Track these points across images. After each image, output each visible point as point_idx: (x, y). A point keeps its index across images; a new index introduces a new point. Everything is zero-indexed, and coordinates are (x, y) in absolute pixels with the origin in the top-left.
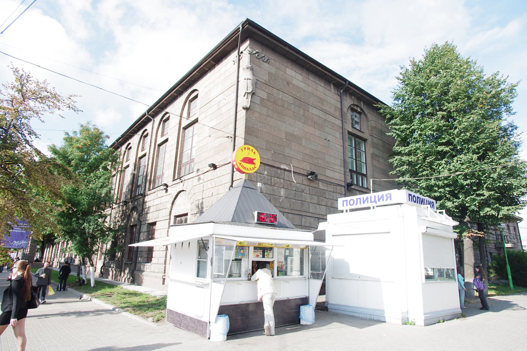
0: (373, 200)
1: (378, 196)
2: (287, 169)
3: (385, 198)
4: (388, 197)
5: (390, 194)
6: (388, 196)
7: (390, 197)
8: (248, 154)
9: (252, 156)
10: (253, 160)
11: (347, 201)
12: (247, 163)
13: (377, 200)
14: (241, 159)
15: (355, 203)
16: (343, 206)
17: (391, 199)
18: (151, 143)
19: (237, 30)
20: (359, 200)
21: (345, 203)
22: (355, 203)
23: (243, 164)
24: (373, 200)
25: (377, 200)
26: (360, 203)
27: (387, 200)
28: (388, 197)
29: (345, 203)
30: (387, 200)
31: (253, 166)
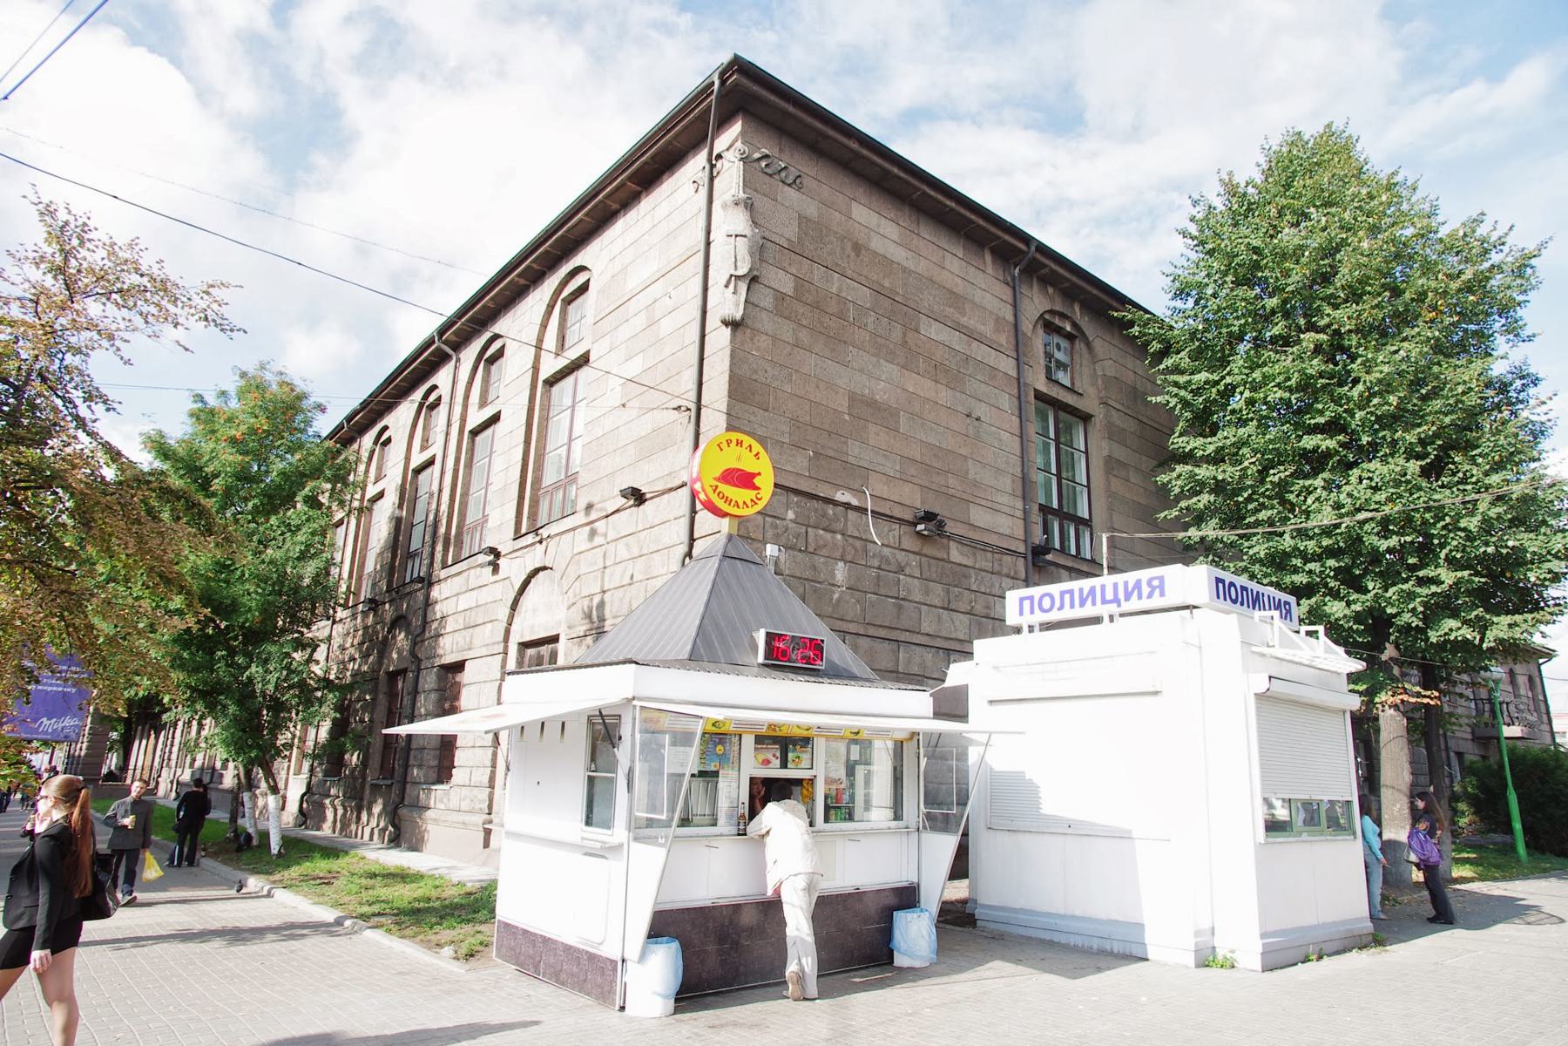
0: (1109, 596)
2: (855, 502)
3: (1146, 590)
4: (1153, 589)
5: (1161, 579)
6: (1156, 583)
8: (739, 459)
9: (749, 465)
10: (754, 475)
11: (1031, 598)
12: (735, 485)
13: (1121, 595)
15: (1057, 604)
16: (1021, 613)
17: (1162, 594)
20: (1067, 597)
21: (1027, 604)
22: (1057, 604)
23: (724, 488)
24: (1109, 596)
25: (1121, 595)
26: (1072, 606)
28: (1153, 589)
29: (1027, 604)
30: (1150, 596)
31: (751, 494)
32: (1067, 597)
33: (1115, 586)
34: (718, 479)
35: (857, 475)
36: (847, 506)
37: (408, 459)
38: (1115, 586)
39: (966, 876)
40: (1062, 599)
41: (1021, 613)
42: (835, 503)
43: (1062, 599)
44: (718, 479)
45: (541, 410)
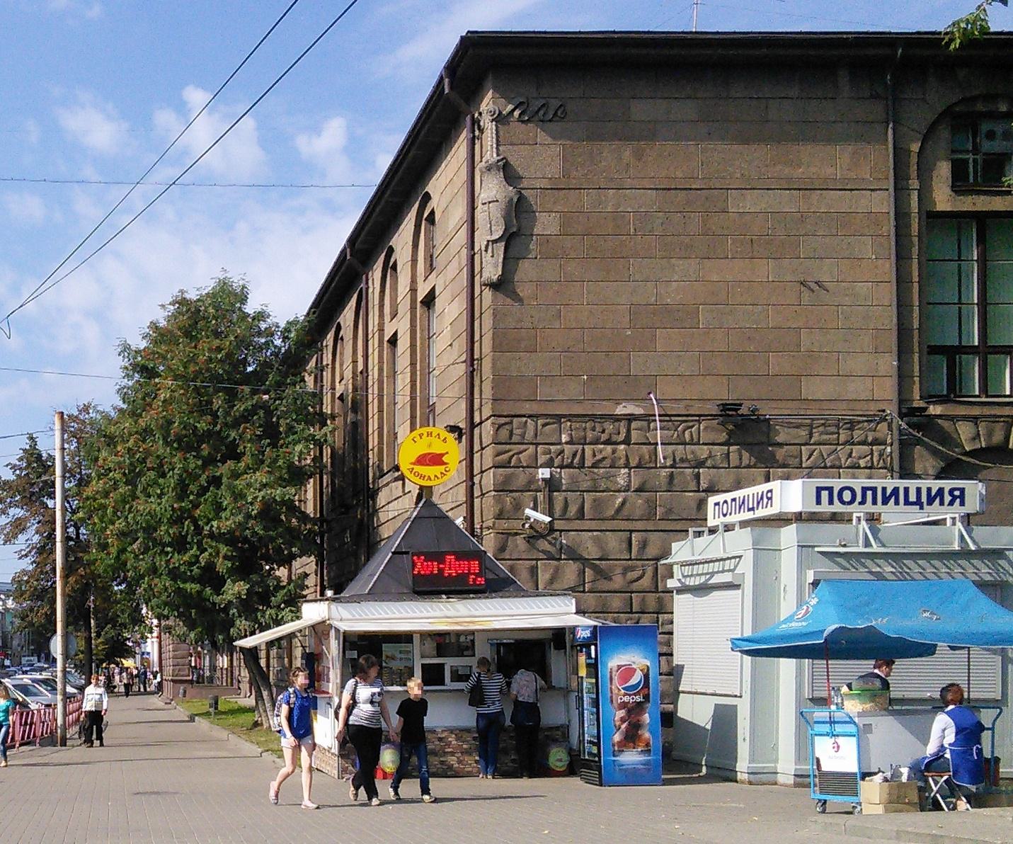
0: (913, 498)
1: (929, 490)
2: (639, 411)
3: (947, 498)
4: (954, 498)
5: (962, 490)
6: (957, 493)
7: (962, 497)
8: (430, 446)
9: (437, 448)
10: (442, 455)
11: (830, 490)
12: (428, 465)
13: (924, 499)
14: (413, 461)
15: (859, 499)
16: (819, 502)
17: (962, 504)
18: (381, 411)
19: (343, 252)
20: (869, 493)
21: (825, 494)
22: (859, 499)
23: (418, 468)
24: (913, 498)
25: (924, 499)
26: (874, 503)
27: (951, 503)
28: (954, 498)
29: (825, 494)
30: (951, 503)
31: (442, 468)
32: (869, 493)
33: (919, 490)
34: (414, 464)
35: (637, 387)
36: (630, 418)
37: (413, 290)
38: (919, 490)
39: (412, 636)
40: (864, 496)
41: (819, 502)
42: (616, 419)
43: (864, 496)
44: (414, 464)
45: (416, 317)
